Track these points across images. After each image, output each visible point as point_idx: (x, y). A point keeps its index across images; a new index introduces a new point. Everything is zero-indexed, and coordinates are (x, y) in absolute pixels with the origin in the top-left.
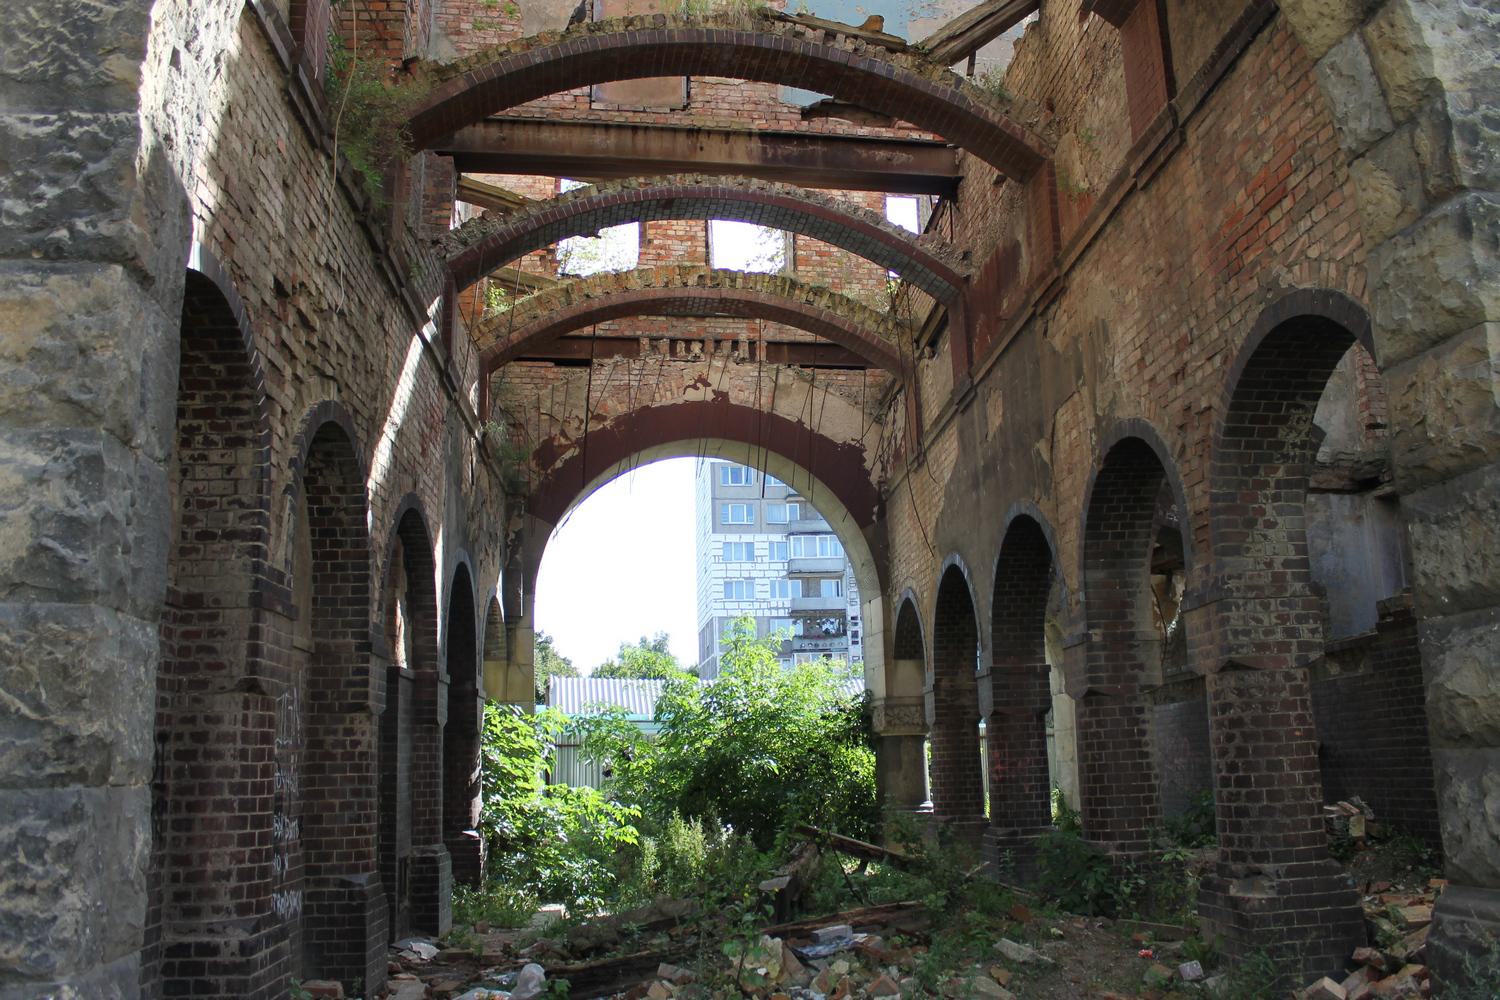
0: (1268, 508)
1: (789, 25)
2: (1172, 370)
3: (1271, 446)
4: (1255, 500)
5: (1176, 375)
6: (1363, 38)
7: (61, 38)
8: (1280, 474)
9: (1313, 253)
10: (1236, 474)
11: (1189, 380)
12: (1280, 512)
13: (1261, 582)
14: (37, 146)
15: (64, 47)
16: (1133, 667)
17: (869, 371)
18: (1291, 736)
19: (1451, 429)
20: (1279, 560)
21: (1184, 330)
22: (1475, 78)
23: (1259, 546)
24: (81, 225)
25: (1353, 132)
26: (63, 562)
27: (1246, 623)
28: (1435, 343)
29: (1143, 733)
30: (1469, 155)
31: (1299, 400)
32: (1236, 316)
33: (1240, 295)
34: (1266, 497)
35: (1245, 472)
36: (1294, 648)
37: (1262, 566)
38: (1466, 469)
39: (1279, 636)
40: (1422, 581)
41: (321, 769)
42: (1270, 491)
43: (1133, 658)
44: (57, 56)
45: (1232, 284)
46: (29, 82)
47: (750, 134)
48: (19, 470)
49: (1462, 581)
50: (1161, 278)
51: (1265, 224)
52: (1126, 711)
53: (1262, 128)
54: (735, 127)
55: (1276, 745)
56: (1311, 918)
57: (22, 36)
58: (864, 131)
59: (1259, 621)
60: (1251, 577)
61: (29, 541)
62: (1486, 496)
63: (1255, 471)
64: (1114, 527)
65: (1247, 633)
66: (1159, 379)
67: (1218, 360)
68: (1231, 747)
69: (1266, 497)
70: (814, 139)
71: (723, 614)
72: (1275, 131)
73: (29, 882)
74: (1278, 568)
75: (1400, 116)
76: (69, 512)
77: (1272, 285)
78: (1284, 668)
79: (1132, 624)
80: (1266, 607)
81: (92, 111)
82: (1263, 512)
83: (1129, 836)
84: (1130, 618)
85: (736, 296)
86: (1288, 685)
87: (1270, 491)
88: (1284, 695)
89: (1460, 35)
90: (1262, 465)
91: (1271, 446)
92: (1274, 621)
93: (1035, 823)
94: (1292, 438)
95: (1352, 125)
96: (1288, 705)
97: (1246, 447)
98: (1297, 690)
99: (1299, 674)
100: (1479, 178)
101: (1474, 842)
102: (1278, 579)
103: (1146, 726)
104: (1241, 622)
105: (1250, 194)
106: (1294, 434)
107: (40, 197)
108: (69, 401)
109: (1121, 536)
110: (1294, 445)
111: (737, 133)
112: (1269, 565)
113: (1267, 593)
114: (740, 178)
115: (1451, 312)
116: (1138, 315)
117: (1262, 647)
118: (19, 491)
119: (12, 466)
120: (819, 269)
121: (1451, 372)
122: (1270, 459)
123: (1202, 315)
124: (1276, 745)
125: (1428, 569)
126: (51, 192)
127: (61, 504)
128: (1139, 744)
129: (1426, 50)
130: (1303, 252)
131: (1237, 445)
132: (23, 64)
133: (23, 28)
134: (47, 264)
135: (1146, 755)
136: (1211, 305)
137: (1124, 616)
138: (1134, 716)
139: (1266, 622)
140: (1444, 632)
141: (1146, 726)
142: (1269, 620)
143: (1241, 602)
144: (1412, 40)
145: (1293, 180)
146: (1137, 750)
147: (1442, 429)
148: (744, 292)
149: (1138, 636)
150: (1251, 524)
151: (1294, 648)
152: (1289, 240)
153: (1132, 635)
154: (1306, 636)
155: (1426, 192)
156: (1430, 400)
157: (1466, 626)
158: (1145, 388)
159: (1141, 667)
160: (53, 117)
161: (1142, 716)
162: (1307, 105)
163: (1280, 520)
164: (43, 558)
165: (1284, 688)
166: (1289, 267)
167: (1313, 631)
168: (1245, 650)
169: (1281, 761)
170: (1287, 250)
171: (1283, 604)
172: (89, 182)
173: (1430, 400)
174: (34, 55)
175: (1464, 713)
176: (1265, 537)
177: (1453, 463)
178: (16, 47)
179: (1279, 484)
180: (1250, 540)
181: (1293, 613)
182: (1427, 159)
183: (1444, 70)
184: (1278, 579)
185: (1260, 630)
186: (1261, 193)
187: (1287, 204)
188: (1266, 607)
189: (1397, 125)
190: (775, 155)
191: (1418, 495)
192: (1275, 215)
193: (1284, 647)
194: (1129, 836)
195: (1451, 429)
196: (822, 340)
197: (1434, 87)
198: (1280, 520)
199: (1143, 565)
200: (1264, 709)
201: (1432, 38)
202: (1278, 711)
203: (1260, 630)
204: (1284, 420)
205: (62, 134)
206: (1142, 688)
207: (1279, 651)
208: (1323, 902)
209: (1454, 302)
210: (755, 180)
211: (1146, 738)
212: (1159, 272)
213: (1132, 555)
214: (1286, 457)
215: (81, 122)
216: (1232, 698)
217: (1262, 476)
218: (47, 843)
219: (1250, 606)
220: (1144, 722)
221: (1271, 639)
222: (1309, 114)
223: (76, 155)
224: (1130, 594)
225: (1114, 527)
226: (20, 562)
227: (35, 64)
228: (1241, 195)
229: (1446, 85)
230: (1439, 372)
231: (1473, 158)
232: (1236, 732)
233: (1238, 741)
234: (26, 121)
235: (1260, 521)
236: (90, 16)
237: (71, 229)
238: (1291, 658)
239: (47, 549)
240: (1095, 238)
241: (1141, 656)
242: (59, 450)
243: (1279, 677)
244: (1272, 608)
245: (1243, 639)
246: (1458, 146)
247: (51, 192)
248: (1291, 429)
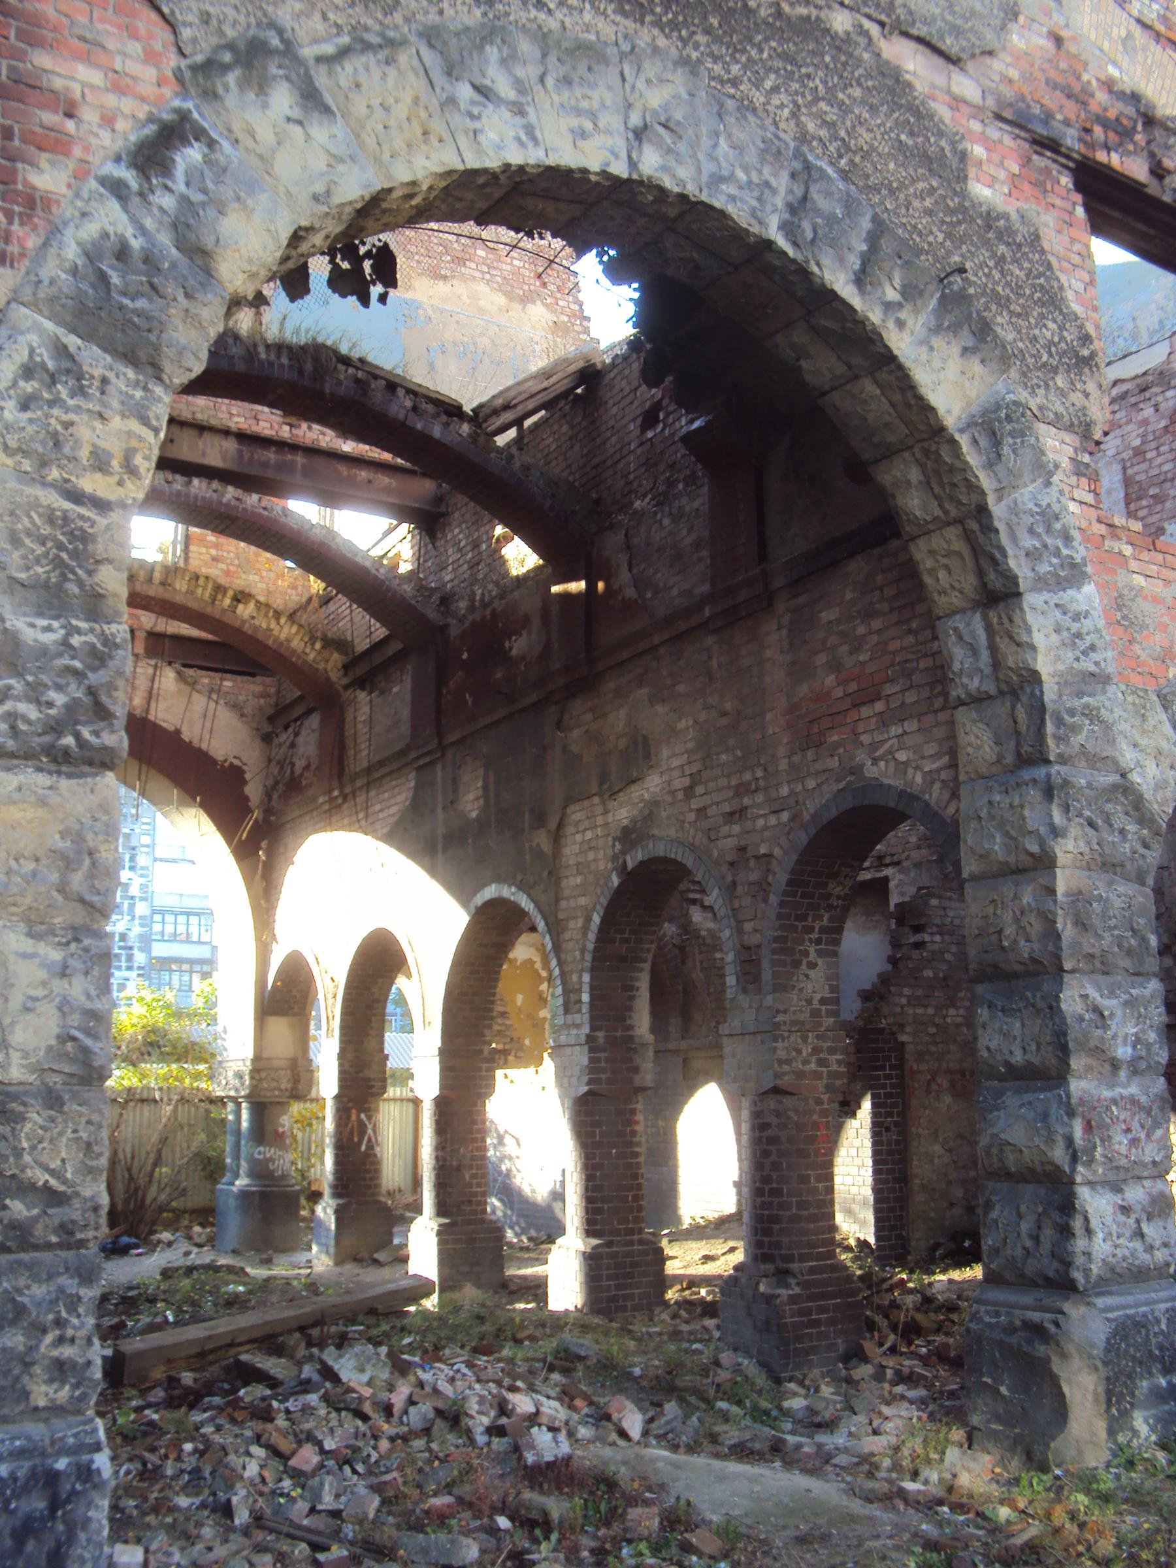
0: (812, 950)
1: (351, 371)
2: (726, 808)
5: (732, 814)
6: (985, 618)
7: (60, 547)
9: (902, 756)
11: (749, 825)
13: (802, 1017)
14: (43, 652)
15: (64, 555)
17: (259, 679)
19: (1022, 943)
20: (817, 997)
21: (747, 776)
22: (1061, 675)
24: (86, 733)
25: (965, 686)
26: (86, 1050)
28: (1013, 872)
30: (1055, 737)
32: (811, 784)
33: (819, 766)
38: (1028, 974)
39: (813, 1066)
40: (985, 1054)
42: (814, 936)
44: (58, 563)
45: (810, 754)
46: (33, 587)
47: (226, 432)
48: (43, 965)
49: (1018, 1058)
50: (724, 721)
51: (854, 715)
53: (861, 630)
54: (213, 422)
56: (821, 1310)
57: (27, 541)
58: (348, 447)
61: (56, 1030)
62: (1043, 998)
63: (804, 917)
64: (622, 932)
66: (710, 812)
67: (785, 816)
68: (767, 1162)
70: (294, 447)
72: (874, 639)
73: (70, 1332)
75: (1004, 687)
76: (89, 1005)
77: (856, 770)
80: (805, 1039)
81: (87, 620)
82: (807, 954)
83: (617, 1233)
85: (152, 593)
87: (814, 936)
89: (1055, 639)
94: (838, 890)
95: (965, 680)
99: (825, 1097)
100: (1060, 755)
101: (1009, 1252)
102: (815, 1013)
105: (843, 683)
107: (50, 704)
108: (82, 901)
109: (628, 940)
111: (212, 429)
112: (809, 1001)
114: (215, 484)
115: (1031, 855)
116: (691, 745)
117: (800, 1074)
118: (44, 984)
119: (37, 961)
120: (213, 552)
121: (1027, 899)
123: (771, 769)
125: (993, 1045)
126: (59, 699)
127: (83, 998)
129: (1033, 648)
130: (890, 752)
132: (28, 568)
133: (29, 534)
134: (53, 767)
135: (636, 1155)
136: (783, 765)
140: (1000, 1094)
144: (1025, 638)
145: (889, 689)
147: (1015, 941)
148: (161, 590)
150: (796, 964)
152: (878, 738)
153: (631, 1038)
155: (1019, 755)
156: (1008, 917)
157: (1018, 1092)
158: (691, 817)
160: (56, 624)
162: (910, 631)
163: (820, 962)
164: (69, 1046)
166: (875, 761)
170: (875, 746)
172: (91, 692)
173: (1008, 917)
174: (38, 561)
175: (1011, 1157)
177: (1019, 968)
178: (22, 551)
179: (823, 930)
182: (1023, 729)
183: (1044, 665)
184: (815, 1013)
186: (853, 687)
187: (879, 706)
188: (805, 1039)
189: (1001, 693)
190: (251, 461)
191: (987, 985)
192: (866, 711)
193: (817, 1075)
194: (617, 1233)
195: (1022, 943)
196: (210, 637)
197: (1035, 677)
198: (820, 962)
201: (1038, 639)
205: (65, 643)
208: (833, 1296)
209: (1035, 848)
210: (230, 489)
212: (724, 714)
214: (831, 907)
215: (78, 631)
216: (773, 1120)
218: (79, 1298)
221: (807, 1068)
222: (911, 639)
223: (77, 664)
225: (622, 932)
226: (50, 1049)
227: (40, 570)
228: (830, 680)
229: (1044, 677)
230: (1016, 897)
231: (1058, 739)
232: (773, 1148)
233: (773, 1157)
234: (33, 626)
236: (86, 525)
237: (77, 736)
238: (821, 1085)
239: (74, 1039)
240: (646, 652)
242: (73, 946)
245: (786, 1068)
246: (1050, 728)
247: (59, 699)
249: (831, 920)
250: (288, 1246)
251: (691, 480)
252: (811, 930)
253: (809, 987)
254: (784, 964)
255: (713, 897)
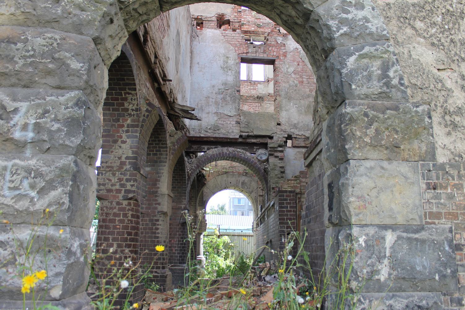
3: (123, 110)
4: (118, 132)
8: (129, 121)
10: (110, 121)
12: (128, 137)
16: (156, 204)
18: (115, 227)
20: (124, 156)
23: (117, 151)
27: (104, 181)
29: (157, 229)
31: (128, 91)
34: (123, 131)
35: (114, 121)
36: (123, 192)
37: (117, 159)
41: (183, 253)
42: (125, 129)
43: (156, 200)
52: (151, 220)
55: (108, 231)
59: (110, 180)
60: (111, 163)
65: (104, 185)
69: (123, 131)
71: (234, 196)
74: (123, 159)
78: (117, 200)
79: (158, 188)
80: (114, 175)
82: (121, 137)
84: (158, 186)
86: (117, 207)
87: (125, 129)
88: (115, 211)
90: (121, 118)
91: (123, 110)
92: (117, 180)
93: (177, 263)
94: (130, 107)
96: (115, 215)
97: (113, 111)
98: (122, 209)
103: (159, 227)
104: (102, 180)
106: (131, 105)
109: (156, 154)
110: (133, 110)
112: (120, 158)
113: (115, 169)
117: (109, 191)
122: (124, 116)
124: (108, 231)
128: (155, 233)
131: (109, 110)
137: (156, 184)
138: (154, 222)
139: (113, 181)
141: (159, 227)
142: (114, 180)
143: (104, 172)
146: (153, 235)
149: (159, 192)
150: (115, 142)
151: (123, 192)
153: (157, 192)
154: (129, 187)
159: (159, 204)
161: (157, 223)
163: (128, 140)
165: (115, 208)
167: (132, 186)
168: (102, 192)
169: (109, 237)
171: (121, 174)
176: (120, 147)
180: (114, 148)
181: (125, 178)
185: (110, 184)
188: (114, 175)
193: (118, 191)
198: (128, 140)
199: (165, 166)
200: (106, 216)
202: (111, 217)
203: (110, 184)
204: (126, 99)
206: (159, 212)
207: (116, 193)
211: (159, 231)
213: (161, 162)
214: (130, 115)
217: (121, 122)
219: (107, 174)
220: (158, 225)
221: (114, 188)
224: (159, 177)
225: (153, 151)
235: (120, 140)
238: (121, 196)
241: (160, 200)
243: (114, 203)
244: (117, 175)
248: (130, 103)
249: (133, 121)
250: (299, 263)
251: (458, 122)
252: (123, 126)
253: (120, 151)
254: (109, 141)
255: (8, 101)
